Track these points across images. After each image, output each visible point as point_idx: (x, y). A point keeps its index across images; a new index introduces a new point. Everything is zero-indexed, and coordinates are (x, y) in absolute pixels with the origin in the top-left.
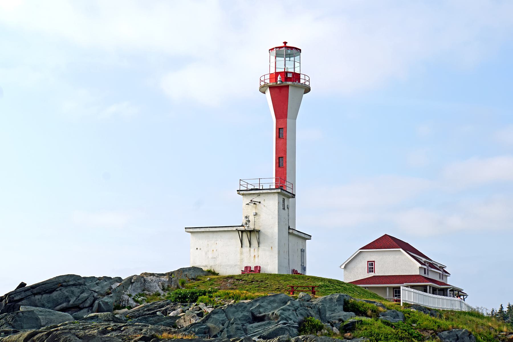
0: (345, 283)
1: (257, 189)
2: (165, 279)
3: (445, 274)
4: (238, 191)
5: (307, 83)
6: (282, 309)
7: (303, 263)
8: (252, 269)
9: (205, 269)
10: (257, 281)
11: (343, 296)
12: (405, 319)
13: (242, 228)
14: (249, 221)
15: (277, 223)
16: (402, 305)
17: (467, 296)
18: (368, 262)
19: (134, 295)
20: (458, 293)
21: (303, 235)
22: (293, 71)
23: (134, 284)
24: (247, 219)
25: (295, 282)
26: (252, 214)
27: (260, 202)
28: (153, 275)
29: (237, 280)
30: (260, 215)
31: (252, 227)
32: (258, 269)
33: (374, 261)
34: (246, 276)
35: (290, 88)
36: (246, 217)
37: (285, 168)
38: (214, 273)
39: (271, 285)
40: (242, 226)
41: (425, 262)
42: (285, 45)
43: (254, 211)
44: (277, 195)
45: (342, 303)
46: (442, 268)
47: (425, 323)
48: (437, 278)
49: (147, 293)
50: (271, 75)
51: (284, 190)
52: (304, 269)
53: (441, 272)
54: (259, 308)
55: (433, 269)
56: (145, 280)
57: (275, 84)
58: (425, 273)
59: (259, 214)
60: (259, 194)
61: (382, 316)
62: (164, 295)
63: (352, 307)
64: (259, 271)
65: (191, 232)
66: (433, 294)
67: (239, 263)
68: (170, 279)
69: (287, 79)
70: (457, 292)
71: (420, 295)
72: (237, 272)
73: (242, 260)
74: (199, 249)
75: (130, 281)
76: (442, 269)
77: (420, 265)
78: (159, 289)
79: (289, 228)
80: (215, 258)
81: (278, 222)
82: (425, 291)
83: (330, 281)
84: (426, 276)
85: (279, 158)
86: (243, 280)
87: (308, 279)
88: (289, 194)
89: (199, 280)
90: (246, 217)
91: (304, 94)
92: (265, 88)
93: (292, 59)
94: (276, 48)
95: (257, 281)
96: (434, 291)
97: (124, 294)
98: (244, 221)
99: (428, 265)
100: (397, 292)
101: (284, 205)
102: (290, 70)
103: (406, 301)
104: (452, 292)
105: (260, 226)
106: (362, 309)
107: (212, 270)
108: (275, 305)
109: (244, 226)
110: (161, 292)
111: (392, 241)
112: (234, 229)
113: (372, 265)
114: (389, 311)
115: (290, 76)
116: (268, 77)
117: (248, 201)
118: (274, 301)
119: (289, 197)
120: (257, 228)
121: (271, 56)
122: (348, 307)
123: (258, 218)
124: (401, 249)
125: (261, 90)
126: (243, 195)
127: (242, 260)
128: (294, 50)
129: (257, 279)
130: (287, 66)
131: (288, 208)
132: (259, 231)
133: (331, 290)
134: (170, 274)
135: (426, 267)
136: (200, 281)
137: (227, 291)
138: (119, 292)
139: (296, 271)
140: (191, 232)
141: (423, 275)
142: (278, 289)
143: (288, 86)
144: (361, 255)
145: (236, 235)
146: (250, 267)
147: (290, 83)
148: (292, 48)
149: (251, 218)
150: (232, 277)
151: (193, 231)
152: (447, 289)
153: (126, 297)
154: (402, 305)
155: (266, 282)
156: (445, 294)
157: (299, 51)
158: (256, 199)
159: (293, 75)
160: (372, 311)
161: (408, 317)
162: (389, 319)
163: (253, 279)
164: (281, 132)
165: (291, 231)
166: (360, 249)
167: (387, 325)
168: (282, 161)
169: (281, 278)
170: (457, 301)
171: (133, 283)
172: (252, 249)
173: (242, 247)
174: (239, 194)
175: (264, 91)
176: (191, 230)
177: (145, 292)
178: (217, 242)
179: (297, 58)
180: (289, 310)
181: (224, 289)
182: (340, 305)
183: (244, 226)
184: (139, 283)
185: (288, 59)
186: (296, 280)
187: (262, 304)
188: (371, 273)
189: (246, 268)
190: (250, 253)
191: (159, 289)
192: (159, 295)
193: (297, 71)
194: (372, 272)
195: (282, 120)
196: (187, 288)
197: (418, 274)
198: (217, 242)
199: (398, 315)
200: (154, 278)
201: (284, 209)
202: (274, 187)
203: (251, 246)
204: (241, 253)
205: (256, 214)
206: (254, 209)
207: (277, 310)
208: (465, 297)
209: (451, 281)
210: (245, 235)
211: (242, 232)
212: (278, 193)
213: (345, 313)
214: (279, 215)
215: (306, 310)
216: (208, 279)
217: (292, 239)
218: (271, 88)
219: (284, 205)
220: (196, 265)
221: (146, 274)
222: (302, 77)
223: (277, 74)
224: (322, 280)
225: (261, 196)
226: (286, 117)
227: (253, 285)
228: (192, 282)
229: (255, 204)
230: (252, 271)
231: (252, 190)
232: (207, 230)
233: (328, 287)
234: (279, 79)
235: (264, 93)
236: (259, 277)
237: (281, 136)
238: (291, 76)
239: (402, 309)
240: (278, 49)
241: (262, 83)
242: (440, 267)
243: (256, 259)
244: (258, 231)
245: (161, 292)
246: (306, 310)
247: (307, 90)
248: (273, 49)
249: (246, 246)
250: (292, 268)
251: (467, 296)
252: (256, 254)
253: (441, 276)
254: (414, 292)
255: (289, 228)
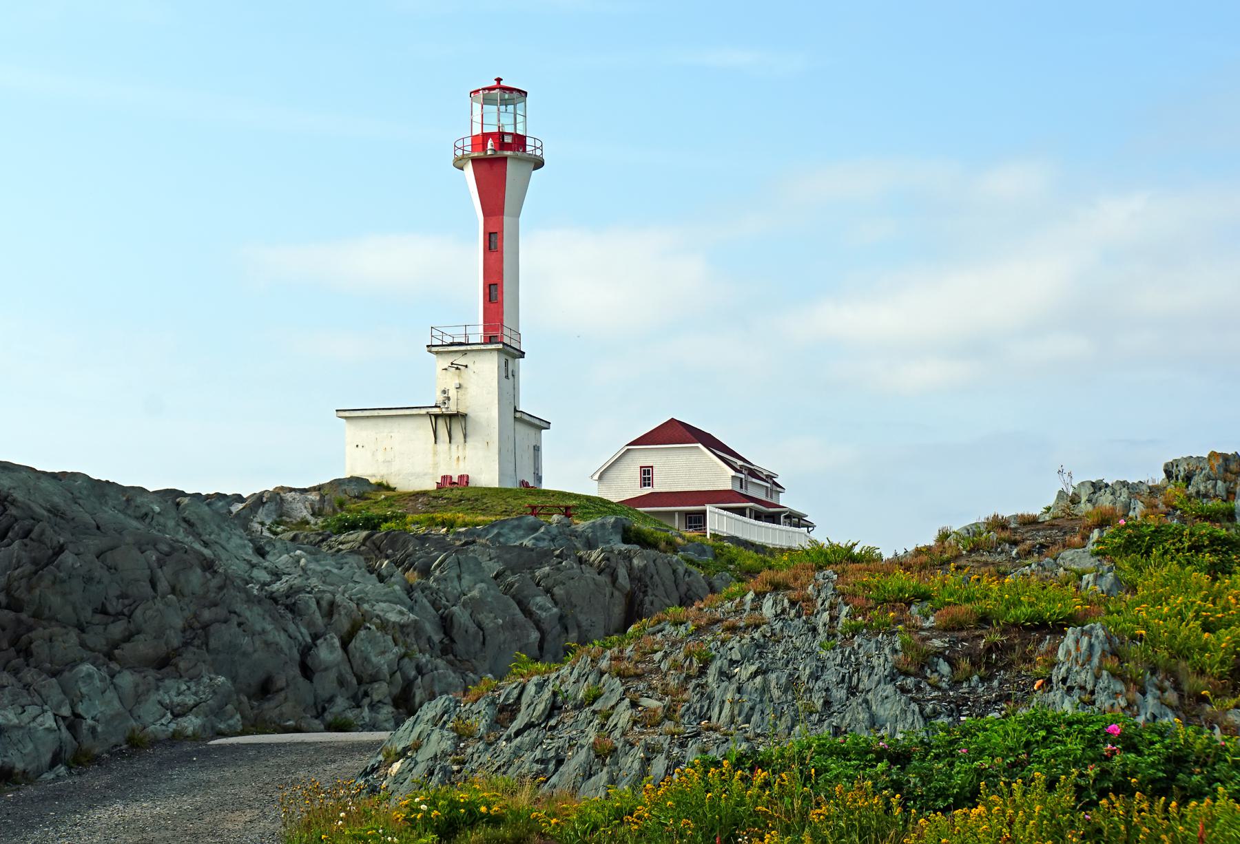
0: (612, 503)
1: (461, 344)
2: (314, 497)
3: (775, 488)
4: (428, 346)
5: (538, 152)
6: (534, 538)
7: (538, 469)
8: (453, 480)
9: (373, 481)
10: (469, 500)
11: (621, 519)
12: (716, 557)
13: (437, 411)
14: (449, 399)
15: (496, 402)
16: (708, 536)
17: (814, 527)
18: (641, 467)
19: (268, 522)
20: (796, 519)
21: (537, 422)
22: (512, 131)
23: (267, 505)
24: (446, 395)
25: (531, 500)
26: (454, 386)
27: (466, 366)
28: (291, 490)
29: (435, 498)
30: (466, 388)
31: (453, 409)
32: (464, 479)
33: (652, 467)
34: (449, 491)
35: (509, 163)
36: (444, 392)
37: (500, 304)
38: (388, 488)
39: (492, 506)
40: (436, 407)
41: (741, 466)
42: (499, 83)
43: (457, 382)
44: (495, 356)
45: (621, 530)
46: (771, 477)
47: (749, 562)
48: (761, 495)
49: (288, 520)
50: (474, 138)
51: (508, 345)
52: (539, 479)
53: (769, 485)
54: (499, 537)
55: (754, 480)
56: (282, 499)
57: (482, 154)
58: (741, 487)
59: (465, 386)
60: (465, 353)
61: (682, 551)
62: (316, 524)
63: (636, 537)
64: (467, 483)
65: (346, 418)
66: (755, 519)
67: (431, 471)
68: (322, 497)
69: (503, 146)
70: (797, 520)
71: (737, 522)
72: (430, 485)
73: (436, 465)
74: (388, 449)
75: (259, 500)
76: (771, 479)
77: (733, 473)
78: (306, 514)
79: (516, 411)
80: (389, 462)
81: (499, 400)
82: (744, 515)
83: (588, 498)
84: (743, 492)
85: (490, 285)
86: (445, 499)
87: (553, 496)
88: (515, 352)
89: (367, 499)
90: (444, 392)
91: (534, 169)
92: (463, 161)
93: (510, 108)
94: (484, 89)
95: (469, 500)
96: (758, 516)
97: (252, 521)
98: (439, 398)
99: (746, 472)
100: (697, 520)
101: (507, 370)
102: (507, 130)
103: (715, 530)
104: (788, 521)
105: (467, 407)
106: (651, 539)
107: (385, 483)
108: (521, 533)
109: (439, 407)
110: (309, 517)
111: (684, 430)
112: (423, 411)
113: (649, 474)
114: (691, 544)
115: (508, 140)
116: (468, 142)
117: (446, 364)
118: (518, 527)
119: (515, 357)
120: (462, 410)
121: (474, 103)
122: (629, 536)
123: (463, 392)
124: (700, 445)
125: (456, 164)
126: (437, 353)
127: (436, 465)
128: (515, 94)
129: (468, 496)
130: (501, 122)
131: (513, 376)
132: (466, 415)
133: (592, 513)
134: (319, 488)
135: (743, 476)
136: (369, 501)
137: (431, 515)
138: (245, 518)
139: (527, 483)
140: (346, 418)
141: (738, 489)
142: (505, 511)
143: (505, 159)
144: (631, 455)
145: (427, 424)
146: (451, 477)
147: (508, 153)
148: (511, 90)
149: (452, 393)
150: (424, 493)
151: (351, 415)
152: (780, 513)
153: (258, 527)
154: (708, 536)
155: (485, 501)
156: (777, 520)
157: (523, 95)
158: (461, 361)
159: (514, 139)
160: (667, 543)
161: (720, 554)
162: (691, 555)
163: (461, 496)
164: (493, 239)
165: (518, 415)
166: (627, 445)
167: (690, 564)
168: (496, 290)
169: (508, 494)
170: (797, 534)
171: (266, 502)
172: (454, 447)
173: (436, 442)
174: (430, 351)
175: (461, 166)
176: (347, 414)
177: (284, 518)
178: (392, 434)
179: (520, 106)
180: (544, 539)
181: (414, 513)
182: (616, 533)
183: (439, 407)
184: (274, 503)
185: (503, 108)
186: (534, 498)
187: (502, 531)
188: (647, 487)
189: (444, 477)
190: (450, 453)
191: (306, 514)
192: (308, 523)
193: (520, 132)
194: (649, 485)
195: (494, 219)
196: (350, 511)
197: (728, 486)
198: (392, 434)
199: (704, 551)
200: (297, 496)
201: (507, 377)
202: (480, 339)
203: (452, 441)
204: (435, 453)
205: (459, 387)
206: (457, 377)
207: (527, 539)
208: (810, 529)
209: (786, 501)
210: (441, 423)
211: (437, 416)
212: (498, 350)
213: (626, 546)
214: (499, 388)
215: (568, 540)
216: (383, 497)
217: (520, 428)
218: (474, 160)
219: (507, 370)
220: (357, 474)
221: (282, 488)
222: (529, 141)
223: (486, 136)
224: (577, 497)
225: (469, 355)
226: (502, 214)
227: (461, 507)
228: (355, 503)
229: (457, 368)
230: (455, 483)
231: (452, 344)
232: (375, 413)
233: (587, 508)
234: (489, 146)
235: (462, 169)
236: (472, 494)
237: (493, 247)
238: (510, 141)
239: (710, 542)
240: (487, 91)
241: (459, 153)
242: (767, 476)
243: (461, 462)
244: (464, 416)
245: (309, 517)
246: (568, 540)
247: (539, 164)
248: (477, 91)
249: (444, 442)
250: (520, 478)
251: (814, 527)
252: (460, 454)
253: (769, 492)
254: (728, 517)
255: (516, 411)
